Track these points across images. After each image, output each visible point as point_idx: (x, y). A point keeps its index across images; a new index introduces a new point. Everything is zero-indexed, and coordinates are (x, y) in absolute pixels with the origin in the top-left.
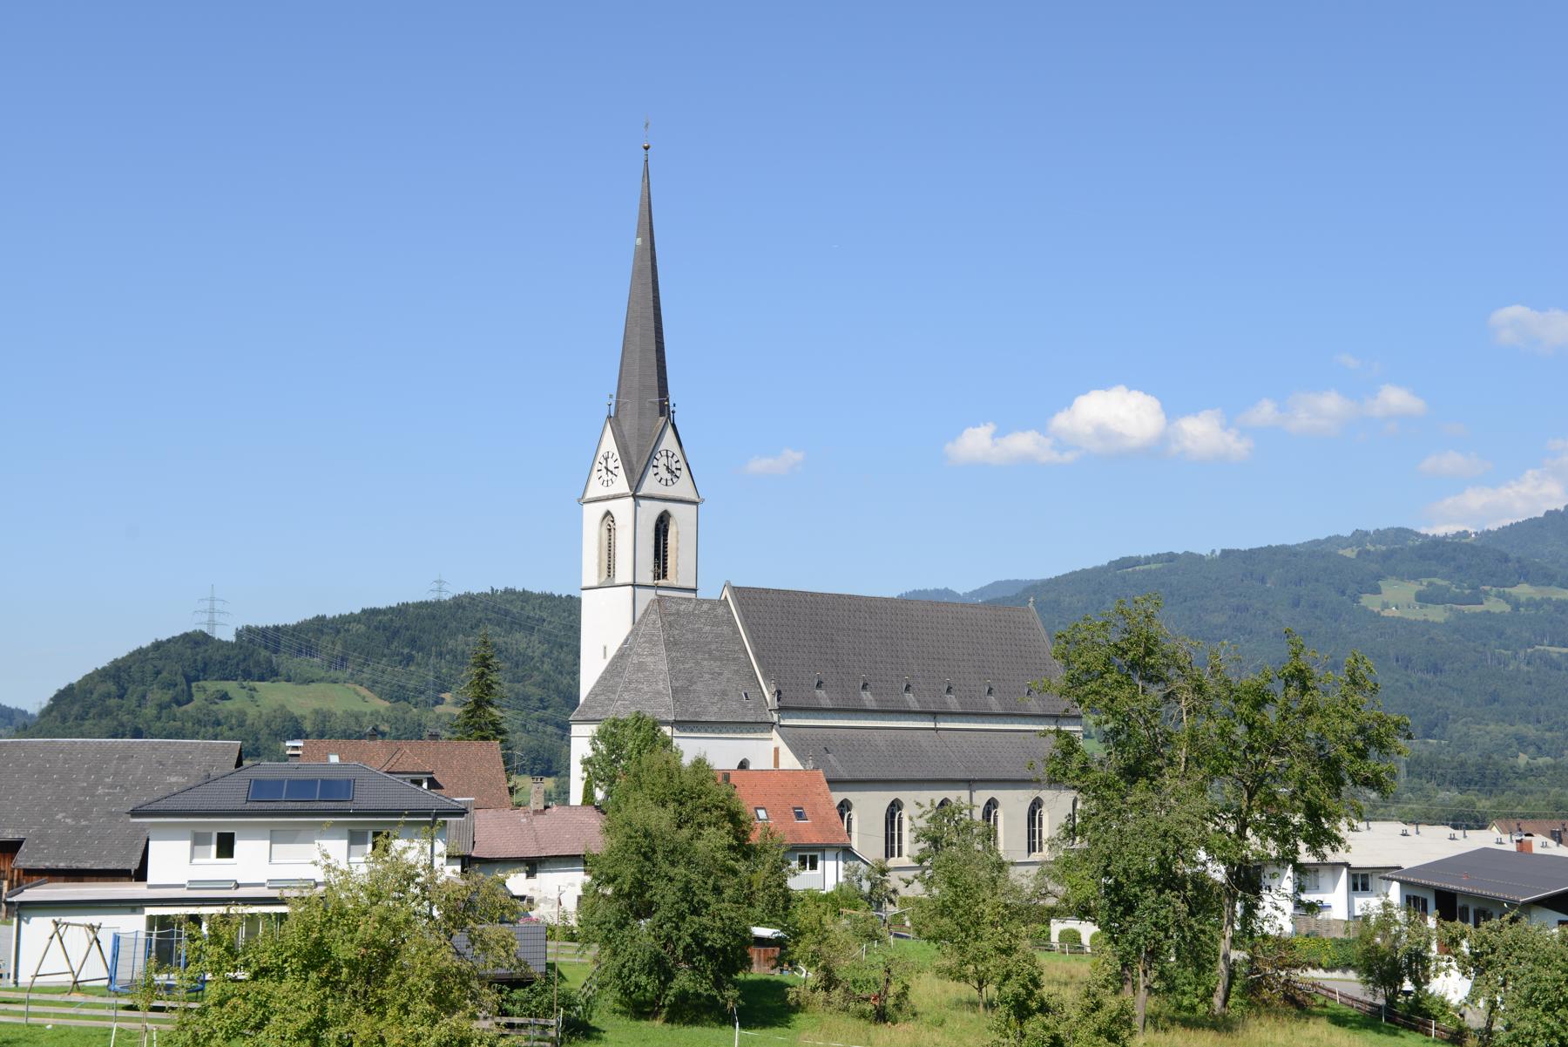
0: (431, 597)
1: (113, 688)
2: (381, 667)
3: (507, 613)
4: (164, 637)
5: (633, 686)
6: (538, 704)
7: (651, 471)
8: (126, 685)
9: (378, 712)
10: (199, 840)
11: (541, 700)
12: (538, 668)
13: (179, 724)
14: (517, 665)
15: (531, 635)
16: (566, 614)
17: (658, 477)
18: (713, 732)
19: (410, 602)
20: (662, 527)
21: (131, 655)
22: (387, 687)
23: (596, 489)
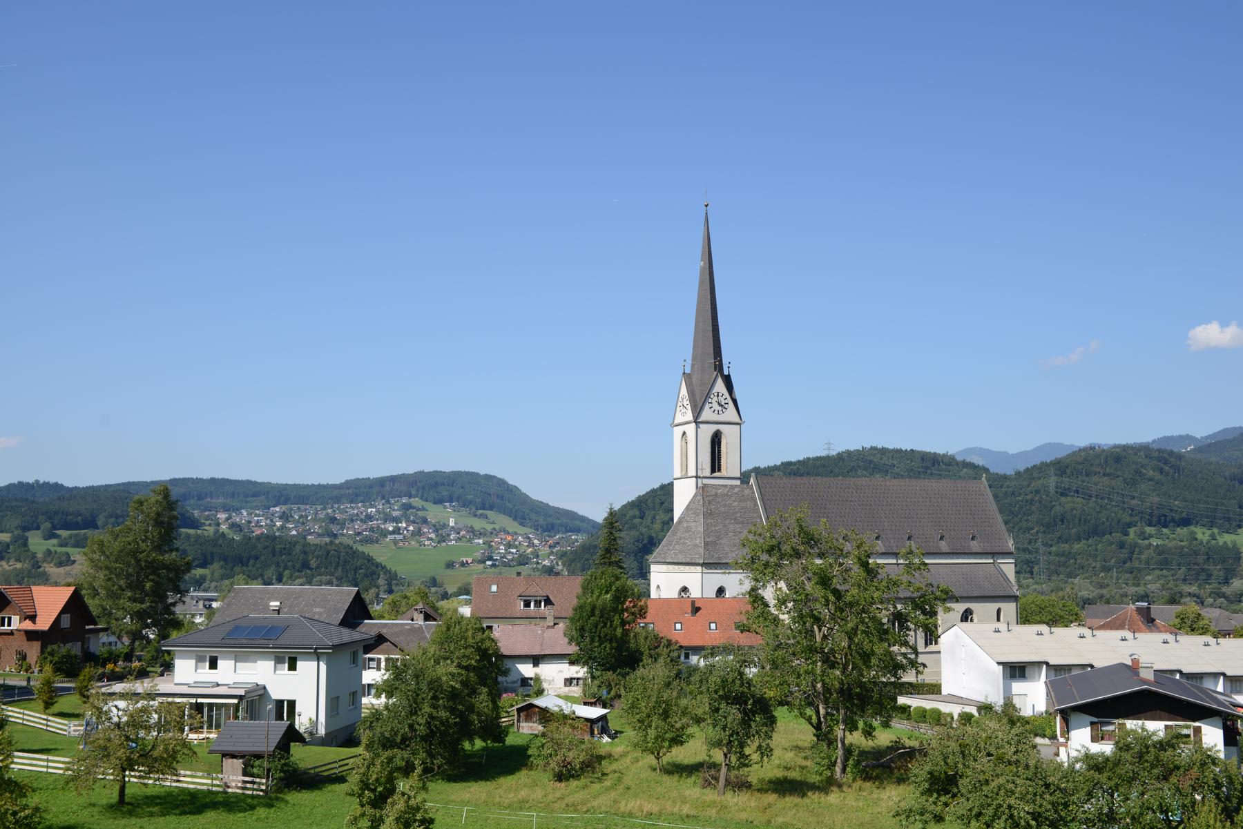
0: (824, 454)
1: (637, 513)
3: (871, 462)
5: (682, 541)
7: (707, 406)
10: (200, 659)
15: (886, 475)
16: (909, 462)
17: (712, 410)
20: (717, 440)
23: (679, 419)
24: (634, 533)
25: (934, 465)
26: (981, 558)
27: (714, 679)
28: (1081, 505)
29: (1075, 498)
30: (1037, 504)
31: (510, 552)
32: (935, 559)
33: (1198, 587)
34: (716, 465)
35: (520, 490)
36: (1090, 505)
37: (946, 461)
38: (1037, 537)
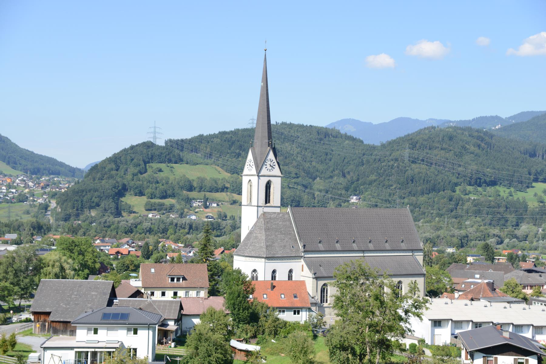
1: (114, 166)
2: (226, 158)
3: (282, 134)
4: (135, 144)
5: (253, 244)
6: (295, 176)
7: (264, 167)
8: (119, 165)
9: (225, 178)
10: (89, 330)
11: (296, 174)
12: (295, 159)
13: (141, 182)
14: (286, 158)
16: (309, 134)
17: (267, 169)
18: (280, 260)
19: (240, 129)
20: (268, 185)
21: (121, 152)
22: (229, 167)
24: (112, 182)
25: (325, 138)
26: (406, 253)
27: (335, 340)
28: (425, 170)
29: (421, 165)
30: (396, 168)
31: (11, 192)
32: (383, 253)
33: (500, 230)
34: (267, 200)
35: (10, 141)
36: (431, 170)
37: (334, 134)
38: (395, 192)
